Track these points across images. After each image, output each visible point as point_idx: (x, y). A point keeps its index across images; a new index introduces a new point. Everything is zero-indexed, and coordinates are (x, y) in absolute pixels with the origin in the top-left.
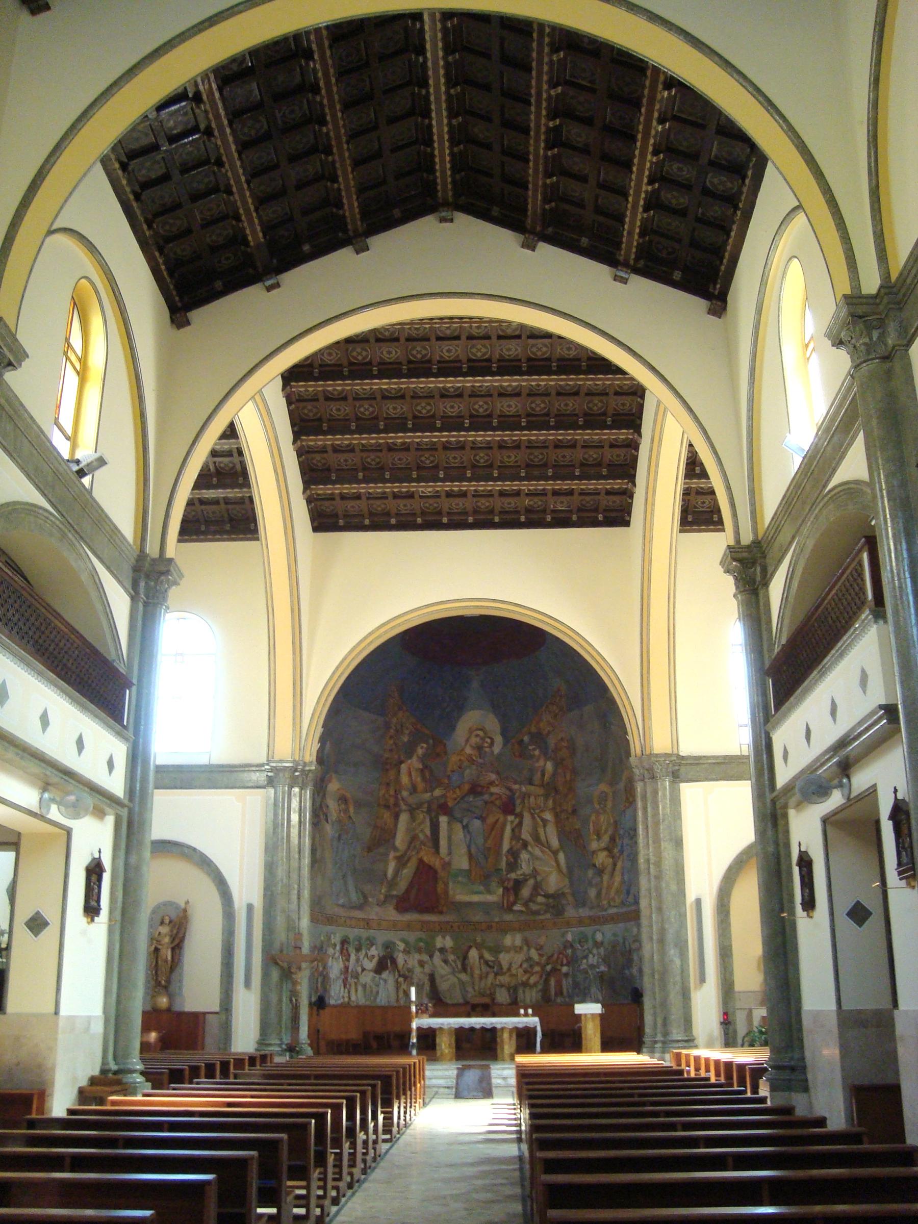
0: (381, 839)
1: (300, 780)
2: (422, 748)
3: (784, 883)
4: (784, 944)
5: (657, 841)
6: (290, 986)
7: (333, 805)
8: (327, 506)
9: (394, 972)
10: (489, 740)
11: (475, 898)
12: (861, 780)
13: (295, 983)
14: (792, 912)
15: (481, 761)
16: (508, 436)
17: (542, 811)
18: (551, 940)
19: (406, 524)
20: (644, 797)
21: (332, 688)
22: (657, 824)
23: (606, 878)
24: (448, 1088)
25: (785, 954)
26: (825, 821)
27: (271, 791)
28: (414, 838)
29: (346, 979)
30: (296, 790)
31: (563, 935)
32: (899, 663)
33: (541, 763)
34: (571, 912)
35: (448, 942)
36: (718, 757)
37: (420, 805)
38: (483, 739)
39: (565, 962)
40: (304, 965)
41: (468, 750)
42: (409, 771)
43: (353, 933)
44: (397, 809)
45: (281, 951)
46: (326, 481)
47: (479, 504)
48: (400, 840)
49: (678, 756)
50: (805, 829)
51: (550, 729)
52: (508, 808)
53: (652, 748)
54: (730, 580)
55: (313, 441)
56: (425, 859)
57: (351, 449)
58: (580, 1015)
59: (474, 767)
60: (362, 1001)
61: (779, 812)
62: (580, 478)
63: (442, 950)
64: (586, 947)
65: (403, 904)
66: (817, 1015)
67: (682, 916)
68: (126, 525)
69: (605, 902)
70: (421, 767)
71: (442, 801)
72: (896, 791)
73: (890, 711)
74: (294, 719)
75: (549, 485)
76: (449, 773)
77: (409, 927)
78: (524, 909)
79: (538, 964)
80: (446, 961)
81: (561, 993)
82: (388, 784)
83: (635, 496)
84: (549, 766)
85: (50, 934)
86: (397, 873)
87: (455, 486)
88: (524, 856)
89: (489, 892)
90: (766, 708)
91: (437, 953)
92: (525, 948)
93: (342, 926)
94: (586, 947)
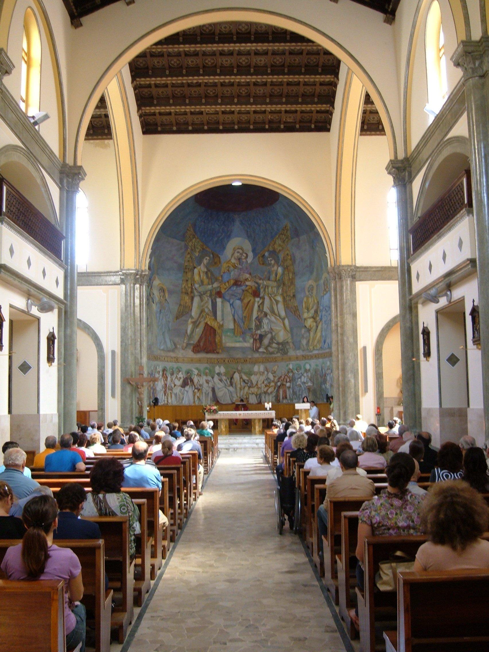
0: (183, 312)
1: (140, 280)
2: (206, 259)
3: (415, 344)
4: (414, 374)
5: (342, 314)
6: (137, 395)
7: (156, 293)
8: (150, 119)
9: (192, 386)
10: (245, 255)
11: (238, 345)
12: (457, 294)
13: (140, 394)
14: (418, 358)
15: (240, 267)
16: (259, 79)
17: (275, 296)
18: (281, 368)
19: (198, 130)
20: (335, 290)
21: (157, 226)
22: (342, 304)
23: (312, 334)
24: (227, 449)
25: (414, 379)
26: (437, 312)
27: (123, 286)
28: (202, 311)
29: (166, 390)
30: (137, 286)
31: (287, 366)
32: (478, 240)
33: (275, 268)
34: (292, 353)
35: (222, 370)
36: (378, 267)
37: (205, 293)
38: (241, 254)
39: (288, 380)
40: (145, 384)
41: (233, 261)
42: (199, 272)
43: (169, 365)
44: (192, 295)
45: (132, 376)
46: (151, 105)
47: (241, 118)
48: (195, 312)
49: (355, 266)
50: (427, 316)
51: (280, 248)
52: (256, 294)
53: (340, 262)
54: (390, 178)
55: (143, 81)
56: (209, 323)
57: (166, 86)
58: (298, 410)
59: (236, 270)
60: (175, 403)
61: (413, 306)
62: (301, 104)
63: (219, 374)
64: (300, 372)
65: (197, 349)
66: (429, 410)
67: (356, 356)
68: (55, 146)
69: (311, 348)
70: (206, 270)
71: (218, 290)
72: (474, 301)
73: (473, 261)
74: (135, 245)
75: (283, 108)
76: (222, 274)
77: (200, 361)
78: (265, 351)
79: (273, 381)
80: (221, 380)
81: (286, 398)
82: (187, 281)
83: (334, 115)
84: (280, 270)
85: (32, 373)
86: (192, 332)
87: (228, 108)
88: (265, 321)
89: (245, 341)
90: (408, 250)
91: (216, 376)
92: (266, 373)
93: (163, 361)
94: (300, 372)
